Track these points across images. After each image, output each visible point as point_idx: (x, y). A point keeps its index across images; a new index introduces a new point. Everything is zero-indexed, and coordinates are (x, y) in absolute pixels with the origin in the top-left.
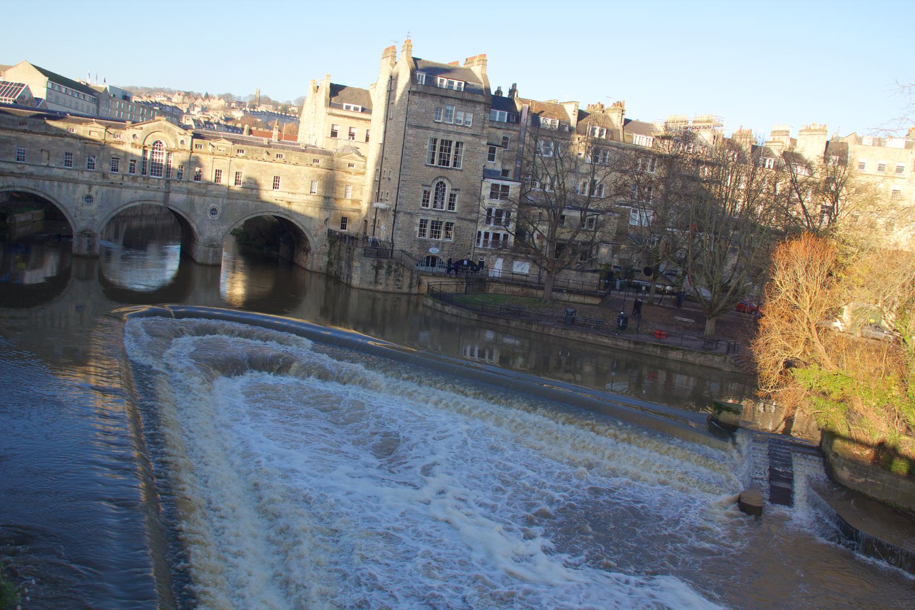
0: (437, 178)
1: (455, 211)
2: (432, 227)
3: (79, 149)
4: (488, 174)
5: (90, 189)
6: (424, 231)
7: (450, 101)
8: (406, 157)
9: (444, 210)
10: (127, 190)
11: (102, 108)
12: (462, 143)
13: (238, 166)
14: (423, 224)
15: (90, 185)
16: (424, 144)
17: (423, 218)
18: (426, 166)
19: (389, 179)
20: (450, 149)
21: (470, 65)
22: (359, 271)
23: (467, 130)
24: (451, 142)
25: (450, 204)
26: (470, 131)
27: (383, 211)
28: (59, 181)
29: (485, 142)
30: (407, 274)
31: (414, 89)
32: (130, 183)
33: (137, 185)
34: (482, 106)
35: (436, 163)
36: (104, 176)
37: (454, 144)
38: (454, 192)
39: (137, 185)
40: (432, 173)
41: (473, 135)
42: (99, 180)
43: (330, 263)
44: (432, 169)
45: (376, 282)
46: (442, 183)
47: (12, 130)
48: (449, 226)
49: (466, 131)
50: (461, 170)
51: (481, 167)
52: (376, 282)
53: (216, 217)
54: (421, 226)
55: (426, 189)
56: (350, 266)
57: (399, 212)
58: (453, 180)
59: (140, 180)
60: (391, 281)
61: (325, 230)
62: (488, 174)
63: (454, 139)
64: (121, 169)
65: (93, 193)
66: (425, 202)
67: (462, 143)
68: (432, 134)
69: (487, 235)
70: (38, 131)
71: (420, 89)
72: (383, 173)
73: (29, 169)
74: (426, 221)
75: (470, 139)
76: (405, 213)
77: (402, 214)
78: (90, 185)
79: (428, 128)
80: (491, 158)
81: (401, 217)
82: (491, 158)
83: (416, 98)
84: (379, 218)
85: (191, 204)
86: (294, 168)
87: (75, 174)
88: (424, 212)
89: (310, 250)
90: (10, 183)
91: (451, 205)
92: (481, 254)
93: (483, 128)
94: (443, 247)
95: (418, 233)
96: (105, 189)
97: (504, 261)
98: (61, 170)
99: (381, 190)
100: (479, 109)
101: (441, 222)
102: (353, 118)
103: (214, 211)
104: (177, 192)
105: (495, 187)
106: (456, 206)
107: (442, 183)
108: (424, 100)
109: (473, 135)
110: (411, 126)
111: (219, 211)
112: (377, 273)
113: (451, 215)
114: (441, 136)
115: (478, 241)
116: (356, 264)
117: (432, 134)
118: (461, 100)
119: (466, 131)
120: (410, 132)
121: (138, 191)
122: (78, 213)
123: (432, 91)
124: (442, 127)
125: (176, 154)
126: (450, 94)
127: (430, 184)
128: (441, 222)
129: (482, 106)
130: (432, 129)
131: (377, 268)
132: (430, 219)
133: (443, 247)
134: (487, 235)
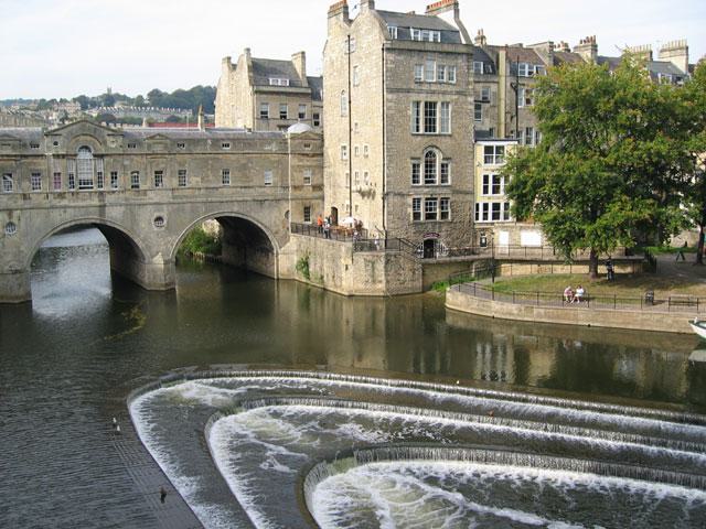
1: (449, 183)
2: (427, 204)
5: (10, 216)
7: (430, 56)
9: (421, 184)
10: (54, 211)
12: (448, 104)
14: (416, 202)
15: (10, 212)
16: (407, 109)
17: (416, 197)
18: (413, 135)
21: (435, 13)
24: (435, 104)
25: (442, 176)
26: (454, 89)
29: (471, 99)
31: (389, 46)
32: (57, 202)
33: (64, 202)
35: (422, 131)
36: (25, 197)
37: (439, 105)
38: (445, 162)
39: (64, 202)
41: (458, 93)
42: (21, 202)
44: (419, 138)
45: (374, 281)
46: (431, 152)
48: (444, 201)
49: (449, 89)
50: (450, 136)
51: (471, 127)
55: (416, 162)
58: (443, 147)
62: (480, 136)
63: (439, 99)
65: (15, 220)
67: (448, 104)
68: (414, 97)
69: (486, 206)
72: (353, 151)
74: (419, 200)
76: (395, 194)
77: (391, 197)
78: (10, 212)
79: (408, 91)
81: (391, 198)
83: (391, 57)
85: (134, 221)
91: (444, 180)
93: (468, 83)
94: (440, 227)
97: (510, 235)
100: (461, 61)
101: (436, 199)
102: (282, 93)
103: (159, 219)
104: (112, 205)
105: (488, 150)
106: (449, 178)
107: (431, 152)
108: (401, 58)
109: (458, 93)
110: (390, 91)
112: (373, 268)
113: (445, 190)
114: (423, 98)
115: (477, 214)
117: (414, 97)
118: (441, 53)
119: (449, 89)
120: (390, 96)
121: (68, 210)
124: (425, 87)
126: (429, 47)
129: (464, 56)
132: (423, 197)
133: (440, 227)
134: (486, 206)
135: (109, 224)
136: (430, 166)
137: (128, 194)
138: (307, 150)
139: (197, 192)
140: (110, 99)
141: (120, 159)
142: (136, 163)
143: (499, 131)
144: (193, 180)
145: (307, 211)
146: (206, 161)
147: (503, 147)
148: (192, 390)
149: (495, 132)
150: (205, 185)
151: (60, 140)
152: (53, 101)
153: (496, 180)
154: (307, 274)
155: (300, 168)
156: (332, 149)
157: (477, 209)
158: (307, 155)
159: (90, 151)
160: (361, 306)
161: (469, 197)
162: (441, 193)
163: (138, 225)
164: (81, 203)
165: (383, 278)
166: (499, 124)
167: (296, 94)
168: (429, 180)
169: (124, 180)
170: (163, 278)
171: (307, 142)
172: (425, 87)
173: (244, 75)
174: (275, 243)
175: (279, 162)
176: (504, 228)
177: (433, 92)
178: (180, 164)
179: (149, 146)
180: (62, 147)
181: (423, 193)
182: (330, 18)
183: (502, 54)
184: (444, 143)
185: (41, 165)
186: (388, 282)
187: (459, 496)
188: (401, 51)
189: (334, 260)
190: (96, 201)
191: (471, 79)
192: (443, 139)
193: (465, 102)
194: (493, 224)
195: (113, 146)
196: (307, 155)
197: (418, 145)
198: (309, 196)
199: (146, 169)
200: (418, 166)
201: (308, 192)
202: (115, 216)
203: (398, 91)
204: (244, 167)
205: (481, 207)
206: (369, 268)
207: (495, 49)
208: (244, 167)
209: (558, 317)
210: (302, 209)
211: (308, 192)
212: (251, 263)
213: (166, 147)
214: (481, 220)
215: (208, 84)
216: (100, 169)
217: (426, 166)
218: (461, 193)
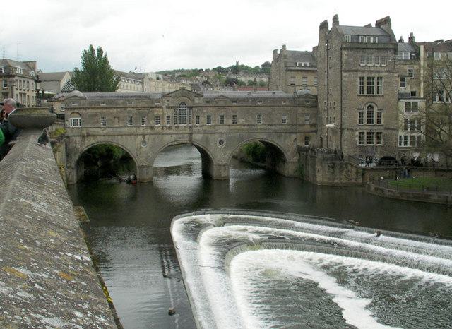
0: (367, 104)
3: (136, 114)
4: (402, 96)
6: (362, 140)
7: (369, 51)
11: (145, 87)
14: (361, 135)
15: (144, 135)
19: (334, 108)
27: (332, 129)
28: (125, 135)
29: (396, 75)
30: (354, 170)
31: (344, 45)
32: (167, 131)
33: (172, 131)
34: (392, 51)
35: (365, 93)
36: (152, 128)
37: (376, 79)
39: (172, 131)
40: (362, 101)
41: (387, 71)
42: (149, 131)
46: (370, 106)
47: (98, 108)
48: (379, 134)
49: (383, 69)
53: (223, 146)
54: (360, 137)
55: (361, 111)
59: (173, 128)
60: (343, 177)
61: (295, 146)
63: (376, 75)
64: (161, 122)
66: (361, 121)
69: (406, 137)
70: (111, 106)
73: (108, 130)
74: (363, 133)
75: (387, 74)
77: (345, 131)
78: (144, 135)
79: (356, 71)
80: (403, 85)
81: (346, 133)
82: (403, 85)
83: (345, 52)
84: (330, 134)
85: (207, 140)
86: (270, 109)
87: (133, 130)
90: (99, 140)
91: (379, 121)
92: (404, 151)
96: (153, 137)
98: (126, 129)
101: (373, 133)
102: (304, 71)
103: (221, 142)
104: (198, 133)
105: (407, 104)
108: (351, 53)
110: (346, 71)
111: (225, 141)
114: (366, 75)
116: (318, 167)
117: (360, 74)
119: (383, 69)
120: (344, 74)
122: (139, 153)
124: (367, 69)
125: (194, 109)
128: (373, 133)
131: (333, 166)
134: (406, 137)
136: (370, 115)
139: (243, 127)
140: (236, 69)
143: (419, 93)
144: (241, 121)
145: (306, 140)
147: (417, 103)
148: (206, 218)
149: (417, 94)
152: (201, 70)
155: (303, 115)
156: (322, 106)
157: (401, 139)
158: (307, 107)
161: (395, 132)
166: (420, 89)
167: (313, 71)
168: (370, 120)
169: (203, 120)
179: (217, 103)
183: (422, 48)
184: (379, 101)
185: (159, 112)
187: (243, 79)
188: (351, 49)
189: (314, 166)
193: (393, 77)
194: (410, 148)
195: (197, 102)
197: (362, 101)
199: (215, 115)
201: (307, 128)
202: (197, 137)
210: (304, 138)
211: (307, 128)
212: (277, 169)
213: (226, 103)
214: (403, 146)
218: (389, 129)
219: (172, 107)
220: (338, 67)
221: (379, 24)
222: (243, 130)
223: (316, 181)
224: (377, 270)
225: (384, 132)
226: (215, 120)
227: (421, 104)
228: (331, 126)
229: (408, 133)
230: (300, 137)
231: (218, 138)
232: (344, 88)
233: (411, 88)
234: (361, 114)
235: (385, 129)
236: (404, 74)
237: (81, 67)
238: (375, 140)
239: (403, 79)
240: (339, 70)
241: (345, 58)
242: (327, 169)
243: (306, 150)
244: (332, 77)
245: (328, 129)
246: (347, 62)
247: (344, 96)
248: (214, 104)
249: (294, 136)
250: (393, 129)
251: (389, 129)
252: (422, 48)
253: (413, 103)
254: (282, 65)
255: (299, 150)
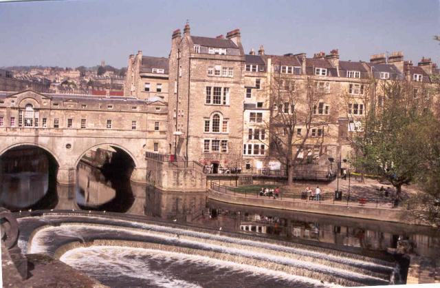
1: (228, 132)
4: (246, 106)
6: (208, 148)
8: (191, 101)
12: (228, 88)
13: (83, 116)
20: (220, 93)
22: (166, 176)
23: (308, 202)
24: (220, 88)
26: (233, 80)
29: (243, 86)
31: (193, 57)
33: (15, 133)
35: (212, 103)
37: (222, 89)
38: (225, 120)
39: (15, 133)
40: (209, 110)
41: (234, 82)
43: (149, 174)
46: (216, 115)
49: (230, 80)
52: (178, 184)
55: (207, 120)
56: (160, 176)
57: (189, 136)
62: (246, 106)
63: (222, 86)
67: (228, 88)
69: (250, 147)
71: (197, 56)
74: (209, 141)
75: (233, 85)
79: (204, 81)
80: (249, 96)
81: (192, 140)
82: (249, 96)
83: (194, 62)
85: (54, 144)
86: (119, 115)
88: (206, 135)
89: (135, 166)
92: (248, 159)
93: (241, 77)
95: (204, 150)
99: (178, 123)
101: (218, 141)
103: (68, 146)
105: (252, 114)
106: (228, 129)
108: (201, 62)
109: (234, 82)
112: (178, 176)
114: (213, 85)
116: (164, 172)
117: (208, 84)
119: (230, 80)
123: (204, 56)
124: (214, 79)
125: (41, 111)
127: (208, 116)
129: (240, 63)
130: (207, 81)
132: (211, 139)
134: (250, 147)
135: (40, 146)
136: (216, 123)
137: (51, 131)
138: (158, 111)
139: (92, 132)
141: (48, 111)
142: (58, 114)
144: (89, 125)
145: (156, 144)
146: (98, 115)
147: (261, 114)
149: (263, 105)
150: (96, 128)
151: (15, 100)
153: (263, 132)
154: (149, 181)
158: (157, 114)
159: (32, 106)
160: (170, 196)
162: (222, 138)
163: (56, 148)
164: (24, 134)
165: (183, 182)
169: (50, 123)
170: (68, 177)
171: (158, 107)
172: (214, 79)
173: (138, 65)
174: (136, 163)
175: (141, 117)
176: (261, 159)
177: (219, 82)
178: (83, 116)
180: (16, 103)
181: (211, 136)
182: (173, 38)
183: (269, 60)
184: (225, 110)
186: (186, 185)
188: (200, 59)
190: (33, 133)
191: (243, 75)
192: (225, 108)
195: (45, 104)
196: (157, 114)
197: (209, 110)
198: (157, 137)
199: (62, 117)
200: (209, 122)
202: (44, 142)
203: (197, 81)
204: (120, 119)
205: (247, 147)
206: (176, 176)
207: (268, 57)
208: (120, 119)
209: (309, 208)
215: (40, 64)
216: (37, 116)
217: (214, 122)
218: (235, 138)
219: (17, 108)
220: (187, 76)
221: (230, 35)
222: (92, 134)
223: (162, 187)
224: (115, 231)
225: (229, 140)
226: (62, 124)
227: (266, 115)
228: (179, 133)
229: (253, 142)
230: (149, 143)
231: (64, 141)
232: (191, 97)
233: (257, 98)
234: (207, 123)
235: (230, 137)
236: (251, 85)
237: (262, 162)
238: (220, 148)
239: (249, 90)
240: (187, 80)
241: (193, 67)
242: (172, 174)
243: (155, 156)
244: (181, 86)
245: (176, 135)
246: (196, 72)
247: (191, 104)
248: (63, 108)
249: (143, 142)
250: (239, 138)
251: (235, 138)
252: (269, 60)
253: (258, 114)
254: (138, 71)
255: (148, 155)
